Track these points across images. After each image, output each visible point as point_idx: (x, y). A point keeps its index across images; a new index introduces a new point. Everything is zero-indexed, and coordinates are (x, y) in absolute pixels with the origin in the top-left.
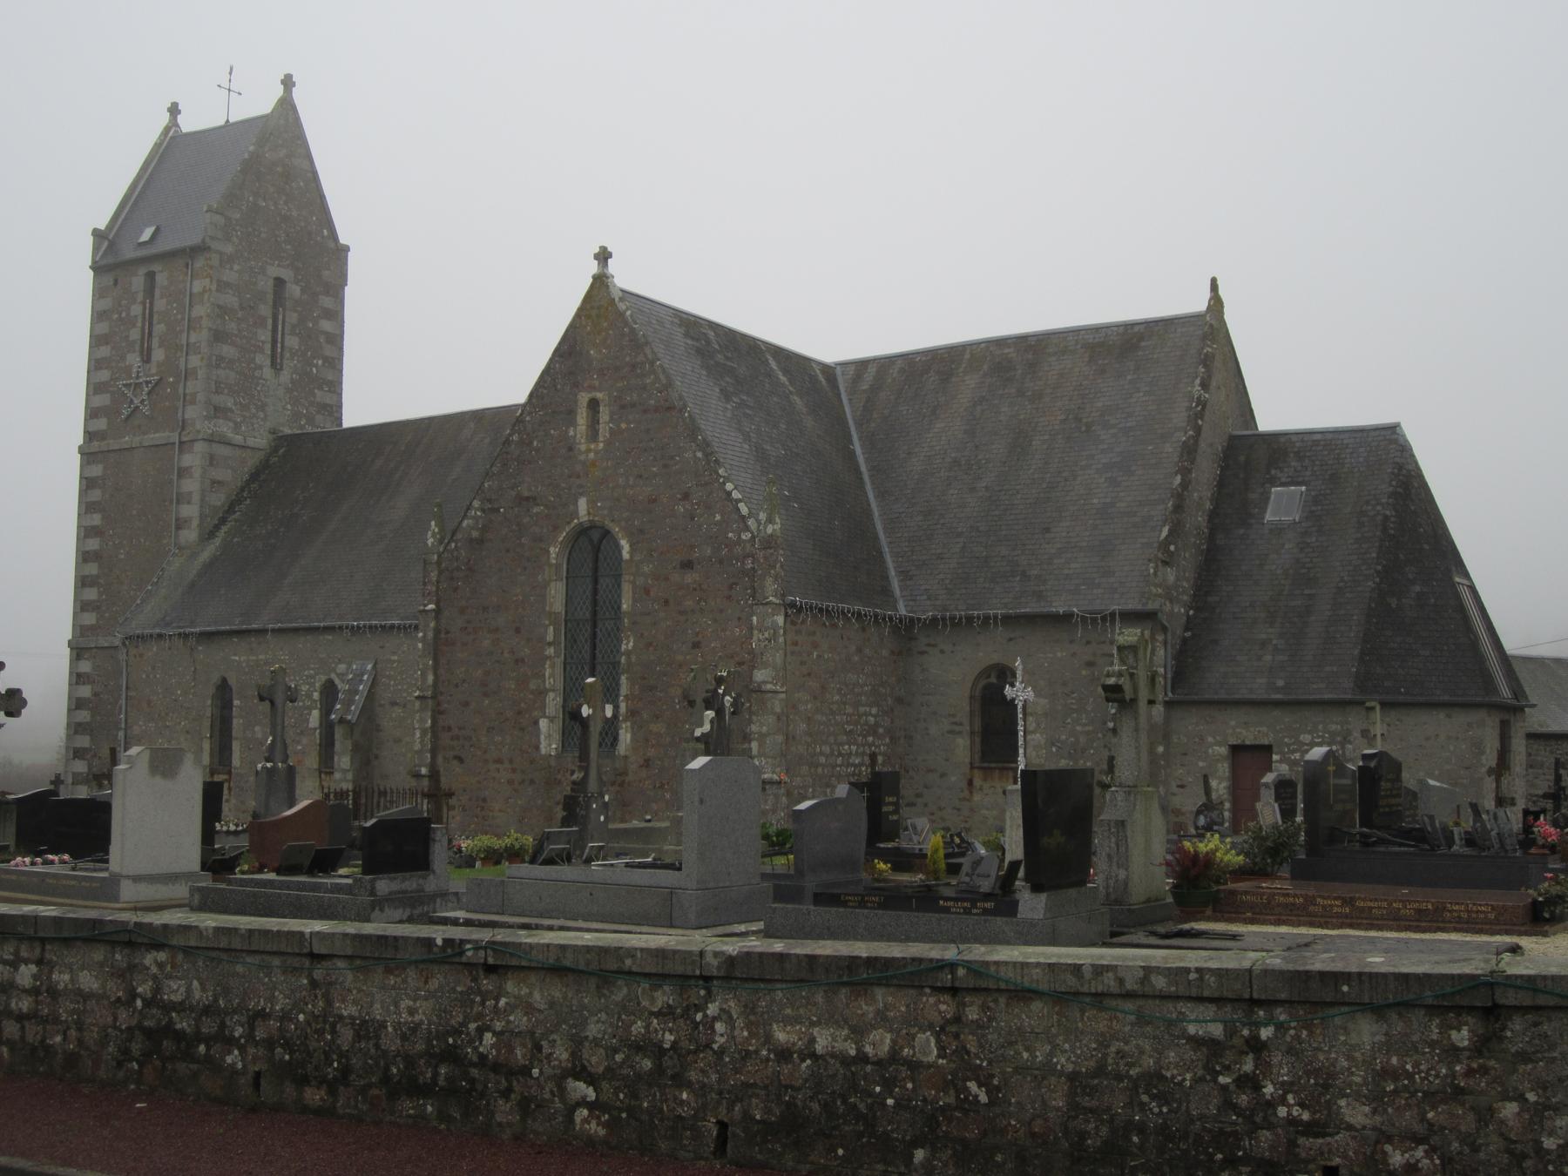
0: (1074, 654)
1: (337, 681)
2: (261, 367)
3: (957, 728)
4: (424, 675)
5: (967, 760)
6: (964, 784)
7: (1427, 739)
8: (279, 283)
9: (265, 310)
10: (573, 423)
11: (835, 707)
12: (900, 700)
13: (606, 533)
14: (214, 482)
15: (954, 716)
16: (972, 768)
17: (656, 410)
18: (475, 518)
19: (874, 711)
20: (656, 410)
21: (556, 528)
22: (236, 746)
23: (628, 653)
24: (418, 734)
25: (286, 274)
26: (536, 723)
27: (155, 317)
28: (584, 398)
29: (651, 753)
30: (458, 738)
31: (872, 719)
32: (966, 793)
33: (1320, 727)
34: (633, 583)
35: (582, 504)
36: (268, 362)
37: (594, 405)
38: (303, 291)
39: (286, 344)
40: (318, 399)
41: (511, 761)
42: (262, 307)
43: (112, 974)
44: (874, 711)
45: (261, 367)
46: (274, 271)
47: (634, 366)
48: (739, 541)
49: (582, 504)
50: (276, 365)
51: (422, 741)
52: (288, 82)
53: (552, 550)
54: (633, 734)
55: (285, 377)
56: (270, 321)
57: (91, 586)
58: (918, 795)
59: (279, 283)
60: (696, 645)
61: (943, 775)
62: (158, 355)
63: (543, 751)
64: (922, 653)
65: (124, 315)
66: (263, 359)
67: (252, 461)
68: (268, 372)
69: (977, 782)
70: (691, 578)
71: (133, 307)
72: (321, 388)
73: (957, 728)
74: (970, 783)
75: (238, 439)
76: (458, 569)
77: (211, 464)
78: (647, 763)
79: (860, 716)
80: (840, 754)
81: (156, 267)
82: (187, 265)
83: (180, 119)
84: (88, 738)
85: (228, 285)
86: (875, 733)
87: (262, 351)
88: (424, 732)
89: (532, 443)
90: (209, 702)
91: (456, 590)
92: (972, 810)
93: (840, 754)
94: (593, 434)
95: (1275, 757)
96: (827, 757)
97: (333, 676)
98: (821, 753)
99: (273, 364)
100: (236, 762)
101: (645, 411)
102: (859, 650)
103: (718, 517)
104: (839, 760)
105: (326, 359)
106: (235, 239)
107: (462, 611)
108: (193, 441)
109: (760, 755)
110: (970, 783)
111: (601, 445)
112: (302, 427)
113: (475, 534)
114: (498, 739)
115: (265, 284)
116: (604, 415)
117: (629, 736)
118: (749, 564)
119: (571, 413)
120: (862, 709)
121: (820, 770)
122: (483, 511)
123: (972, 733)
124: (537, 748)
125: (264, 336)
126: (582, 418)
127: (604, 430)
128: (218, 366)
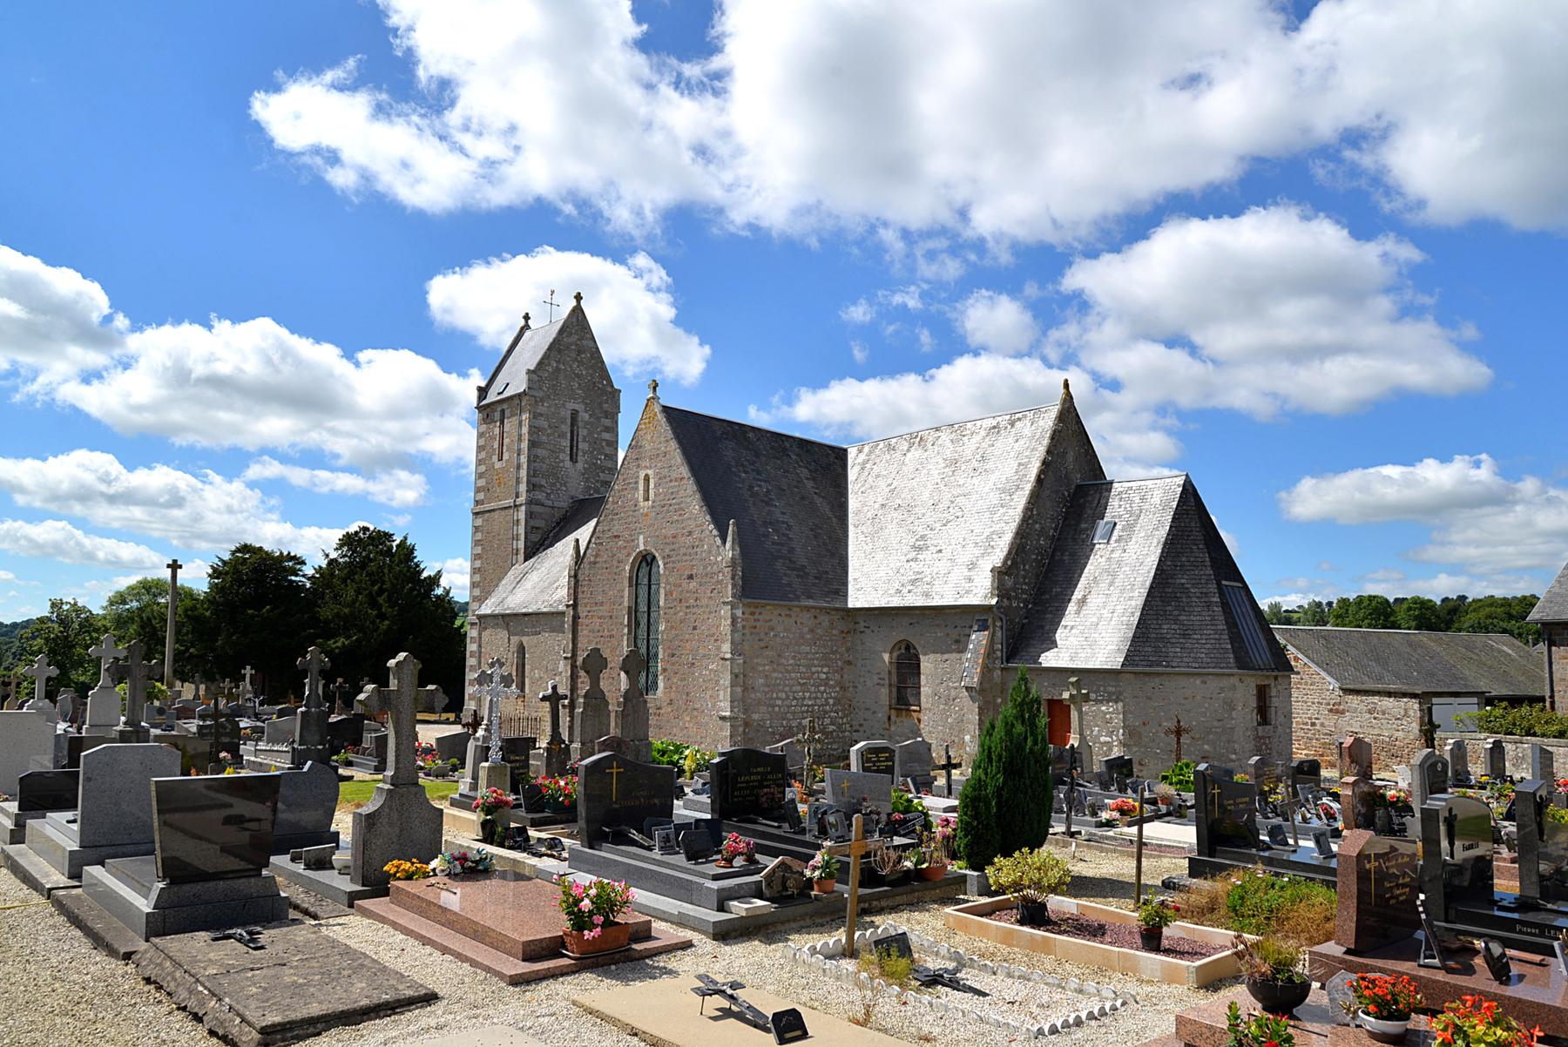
2: (563, 461)
3: (882, 682)
6: (886, 719)
7: (1186, 698)
8: (574, 415)
9: (566, 428)
11: (790, 668)
12: (849, 663)
13: (654, 557)
14: (533, 528)
15: (879, 674)
19: (825, 670)
22: (527, 680)
23: (663, 632)
29: (673, 696)
31: (824, 676)
33: (1102, 689)
36: (568, 458)
37: (647, 478)
39: (580, 447)
40: (602, 478)
44: (825, 670)
45: (563, 461)
46: (571, 405)
48: (716, 562)
50: (573, 458)
52: (578, 297)
55: (580, 465)
56: (569, 435)
58: (861, 725)
61: (874, 713)
64: (862, 632)
68: (568, 464)
69: (893, 718)
70: (693, 584)
72: (603, 472)
73: (882, 682)
74: (889, 718)
75: (550, 503)
77: (531, 518)
78: (671, 702)
79: (814, 673)
80: (795, 698)
81: (505, 406)
83: (530, 322)
85: (541, 415)
86: (826, 685)
93: (795, 698)
96: (783, 700)
98: (778, 698)
102: (812, 631)
104: (794, 703)
105: (606, 455)
106: (545, 389)
110: (889, 718)
112: (592, 495)
120: (814, 669)
121: (777, 709)
123: (890, 685)
125: (566, 443)
128: (535, 461)
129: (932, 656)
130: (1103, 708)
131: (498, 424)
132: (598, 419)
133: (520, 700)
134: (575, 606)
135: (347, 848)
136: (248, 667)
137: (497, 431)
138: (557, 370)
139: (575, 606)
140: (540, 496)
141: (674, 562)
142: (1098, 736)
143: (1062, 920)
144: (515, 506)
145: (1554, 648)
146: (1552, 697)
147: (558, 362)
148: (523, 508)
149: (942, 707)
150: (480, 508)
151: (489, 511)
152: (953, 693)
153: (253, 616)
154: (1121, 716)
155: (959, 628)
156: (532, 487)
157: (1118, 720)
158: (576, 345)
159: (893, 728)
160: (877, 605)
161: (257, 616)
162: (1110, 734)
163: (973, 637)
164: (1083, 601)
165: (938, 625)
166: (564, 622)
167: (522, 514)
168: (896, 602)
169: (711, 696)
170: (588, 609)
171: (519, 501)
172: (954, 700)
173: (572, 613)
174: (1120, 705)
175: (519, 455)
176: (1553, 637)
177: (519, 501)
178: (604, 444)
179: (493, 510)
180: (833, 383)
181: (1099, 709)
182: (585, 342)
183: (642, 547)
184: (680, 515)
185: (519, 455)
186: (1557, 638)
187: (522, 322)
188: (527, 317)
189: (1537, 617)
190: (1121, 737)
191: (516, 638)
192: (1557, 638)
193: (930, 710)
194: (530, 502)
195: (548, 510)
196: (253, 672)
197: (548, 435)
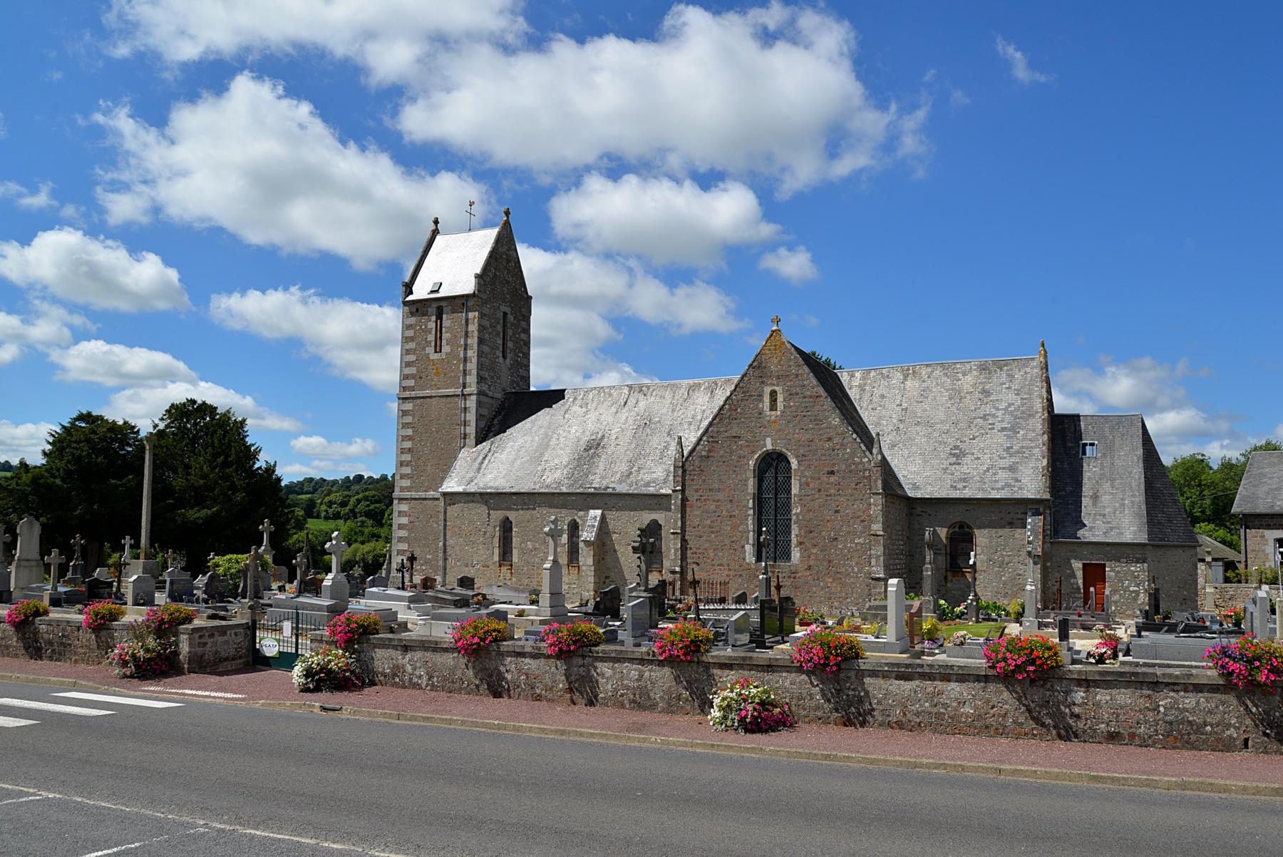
0: (1002, 519)
1: (578, 520)
2: (498, 357)
3: (939, 552)
4: (675, 521)
5: (944, 567)
6: (942, 579)
10: (761, 401)
16: (947, 571)
17: (811, 397)
18: (705, 446)
20: (811, 397)
21: (753, 452)
23: (797, 515)
24: (673, 551)
25: (508, 310)
26: (743, 547)
27: (444, 330)
28: (768, 390)
29: (812, 563)
30: (696, 553)
32: (944, 583)
34: (800, 480)
35: (768, 441)
38: (514, 319)
41: (728, 565)
42: (498, 326)
43: (1033, 681)
45: (498, 357)
46: (503, 308)
47: (797, 375)
48: (861, 463)
49: (768, 441)
50: (504, 357)
51: (675, 554)
53: (750, 462)
54: (801, 554)
55: (508, 361)
56: (502, 334)
57: (407, 465)
59: (505, 314)
60: (837, 512)
62: (446, 349)
63: (748, 561)
65: (423, 327)
66: (499, 353)
67: (496, 404)
68: (501, 359)
69: (950, 578)
70: (832, 479)
71: (429, 323)
73: (939, 552)
74: (946, 578)
76: (694, 470)
81: (443, 304)
82: (463, 304)
84: (407, 545)
85: (485, 315)
87: (498, 348)
88: (676, 550)
89: (737, 409)
90: (498, 529)
91: (693, 480)
92: (947, 591)
94: (773, 407)
95: (1107, 569)
97: (576, 517)
99: (503, 357)
100: (515, 559)
101: (805, 397)
103: (848, 450)
107: (697, 491)
108: (470, 395)
109: (876, 566)
110: (946, 578)
111: (779, 413)
113: (704, 453)
114: (720, 554)
115: (500, 315)
116: (780, 398)
117: (798, 554)
118: (867, 474)
119: (761, 396)
122: (709, 442)
123: (946, 554)
124: (744, 559)
126: (767, 399)
127: (780, 405)
129: (986, 531)
130: (1132, 568)
131: (434, 318)
132: (519, 321)
133: (504, 569)
134: (683, 491)
135: (874, 674)
136: (128, 538)
137: (432, 325)
138: (495, 275)
139: (683, 491)
140: (485, 388)
141: (810, 460)
142: (1128, 587)
143: (892, 728)
144: (463, 395)
145: (1248, 530)
146: (1246, 561)
147: (495, 269)
148: (474, 398)
149: (996, 569)
150: (407, 394)
151: (423, 398)
152: (1007, 559)
153: (116, 487)
154: (1146, 573)
155: (1012, 514)
156: (481, 379)
157: (1144, 576)
158: (506, 255)
159: (949, 585)
160: (937, 495)
161: (120, 485)
162: (1137, 586)
163: (1030, 520)
164: (1095, 497)
165: (993, 512)
166: (670, 504)
167: (472, 403)
168: (943, 494)
169: (857, 563)
170: (700, 493)
171: (467, 391)
172: (1007, 564)
173: (680, 497)
174: (1146, 565)
175: (465, 349)
176: (1248, 523)
177: (467, 391)
178: (522, 343)
179: (430, 397)
180: (39, 233)
181: (1129, 569)
182: (511, 252)
183: (769, 447)
184: (818, 424)
185: (465, 349)
186: (1250, 524)
187: (433, 227)
188: (436, 222)
189: (1239, 510)
190: (1146, 587)
191: (500, 513)
192: (1250, 524)
193: (985, 571)
194: (480, 393)
195: (490, 400)
196: (133, 542)
197: (490, 334)
